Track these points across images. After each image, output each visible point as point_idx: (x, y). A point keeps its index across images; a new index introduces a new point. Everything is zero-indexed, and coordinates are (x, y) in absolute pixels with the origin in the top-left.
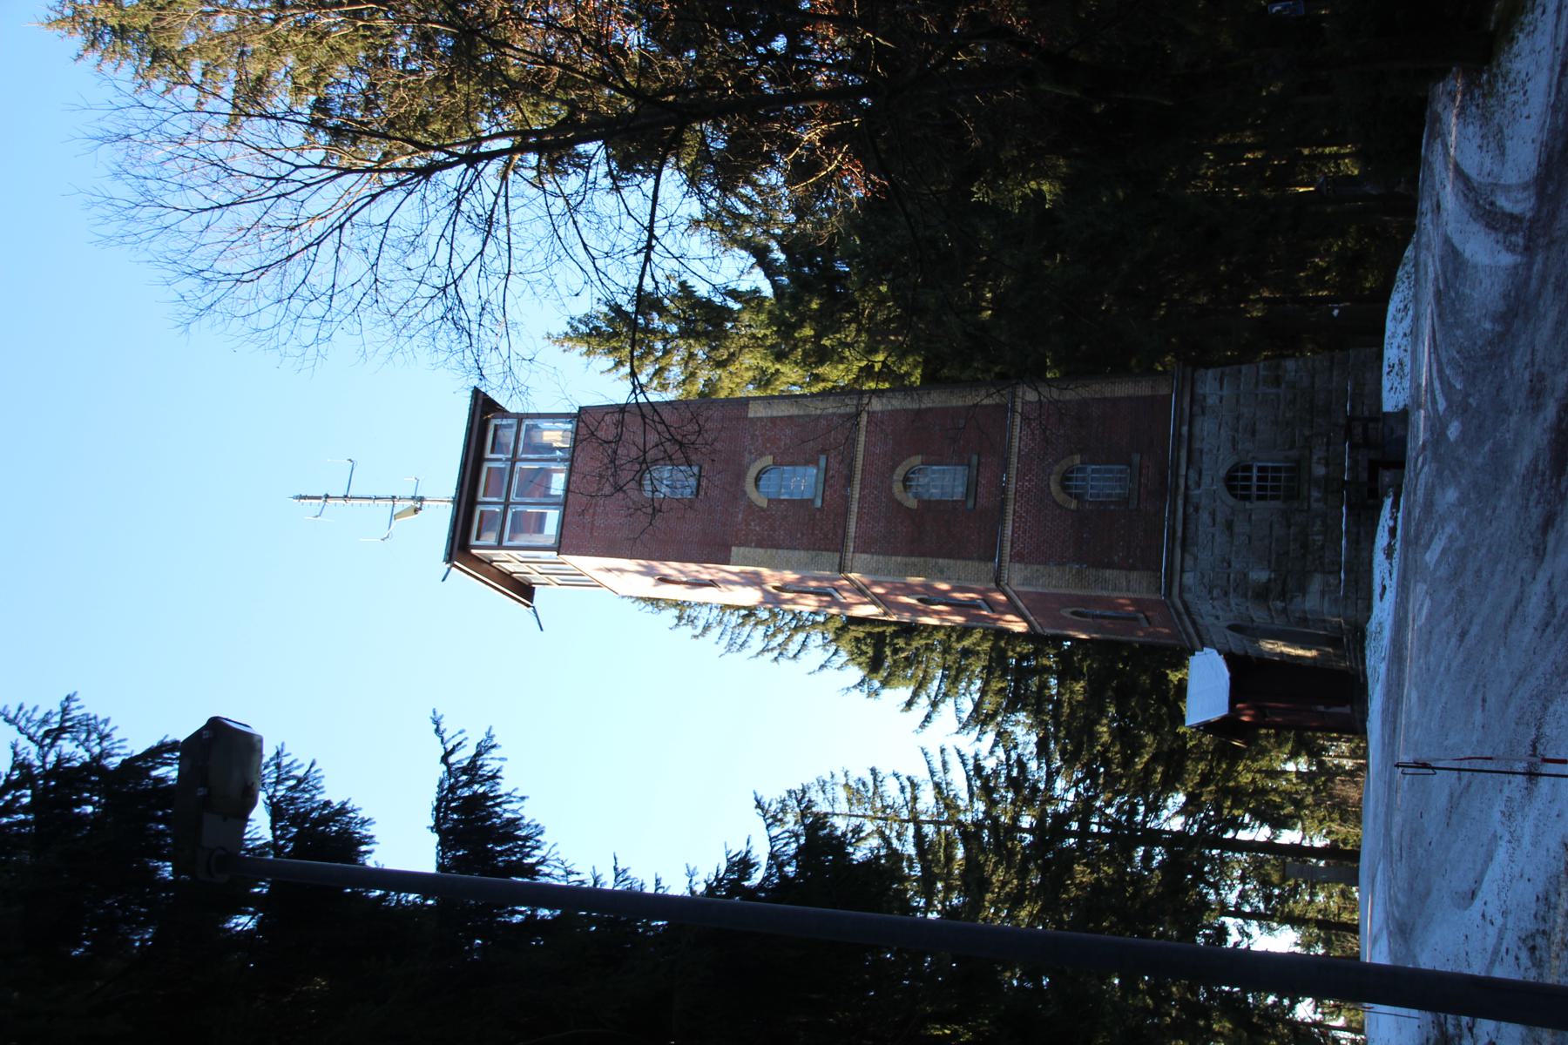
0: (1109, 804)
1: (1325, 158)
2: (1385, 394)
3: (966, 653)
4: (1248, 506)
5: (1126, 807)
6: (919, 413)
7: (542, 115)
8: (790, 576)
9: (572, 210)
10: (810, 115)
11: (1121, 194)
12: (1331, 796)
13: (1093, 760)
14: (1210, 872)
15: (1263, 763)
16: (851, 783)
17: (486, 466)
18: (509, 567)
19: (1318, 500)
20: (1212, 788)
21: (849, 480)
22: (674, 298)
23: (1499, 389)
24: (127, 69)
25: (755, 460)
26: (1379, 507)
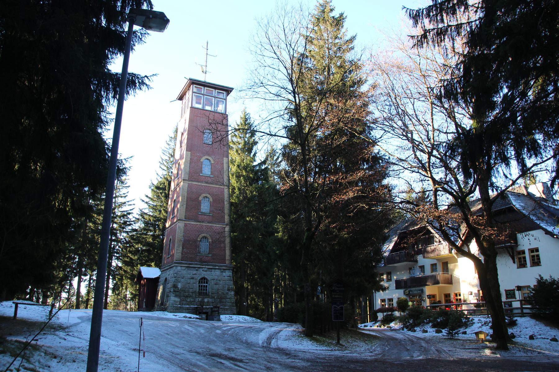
0: (119, 247)
3: (160, 211)
5: (118, 251)
8: (182, 167)
11: (277, 252)
12: (120, 303)
15: (129, 286)
16: (126, 180)
17: (214, 90)
20: (123, 273)
21: (207, 183)
26: (196, 314)
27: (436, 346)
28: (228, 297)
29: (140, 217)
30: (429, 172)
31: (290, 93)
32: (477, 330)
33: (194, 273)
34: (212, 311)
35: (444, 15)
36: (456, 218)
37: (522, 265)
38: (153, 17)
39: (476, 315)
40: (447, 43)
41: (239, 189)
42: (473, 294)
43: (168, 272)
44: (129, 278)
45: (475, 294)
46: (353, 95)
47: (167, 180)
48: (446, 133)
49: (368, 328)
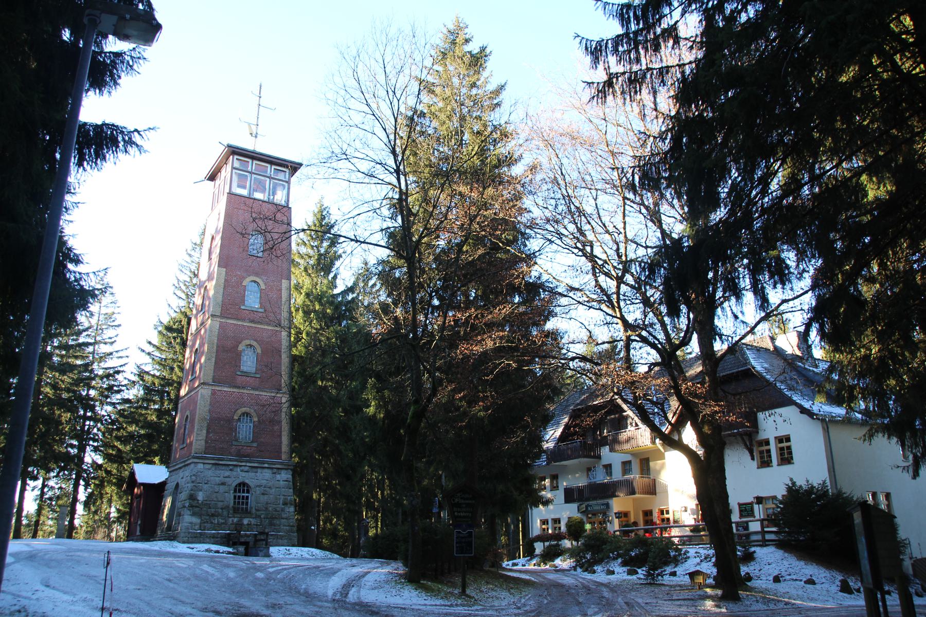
0: (99, 430)
1: (376, 522)
2: (277, 548)
3: (172, 369)
4: (232, 492)
6: (279, 352)
7: (414, 202)
8: (211, 293)
9: (375, 211)
10: (406, 312)
12: (98, 527)
13: (120, 423)
14: (64, 473)
15: (115, 498)
17: (269, 166)
18: (223, 171)
19: (233, 521)
20: (104, 475)
21: (252, 321)
22: (335, 252)
23: (276, 592)
24: (441, 44)
26: (228, 546)
27: (625, 597)
28: (284, 516)
29: (136, 379)
30: (617, 310)
31: (391, 173)
32: (692, 569)
33: (226, 475)
34: (256, 541)
35: (642, 52)
36: (659, 386)
37: (765, 463)
38: (131, 19)
39: (693, 545)
40: (645, 95)
41: (308, 334)
42: (689, 511)
43: (181, 473)
44: (115, 484)
45: (692, 510)
46: (497, 181)
47: (186, 315)
48: (646, 247)
49: (519, 567)
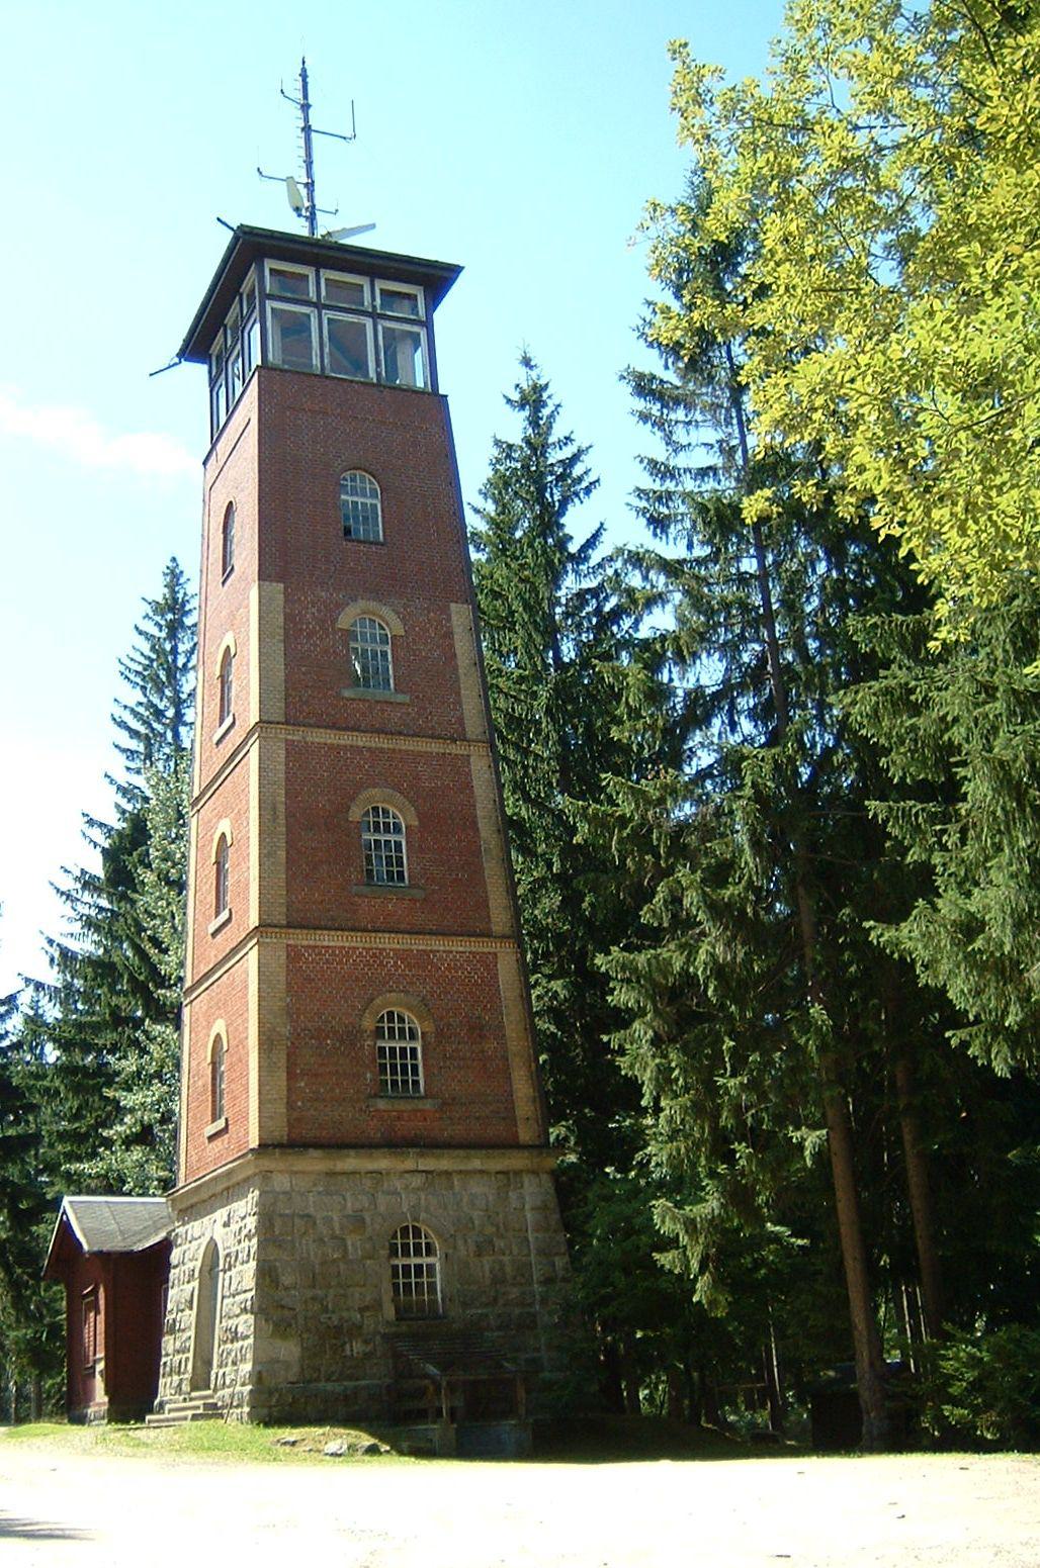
25: (398, 613)
